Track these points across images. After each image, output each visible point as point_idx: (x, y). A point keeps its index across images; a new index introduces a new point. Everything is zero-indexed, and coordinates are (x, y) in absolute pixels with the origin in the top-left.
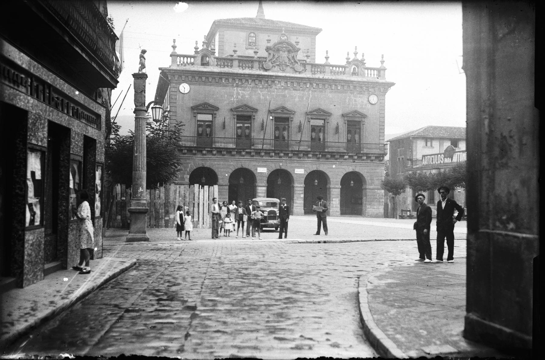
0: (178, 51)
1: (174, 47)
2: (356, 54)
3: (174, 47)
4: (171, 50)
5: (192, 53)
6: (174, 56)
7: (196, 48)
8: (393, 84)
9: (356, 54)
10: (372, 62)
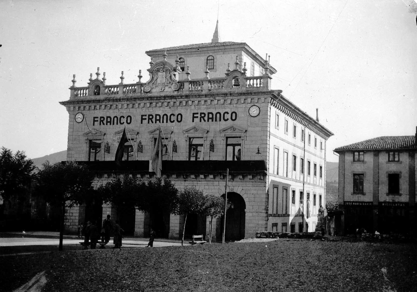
0: (77, 85)
1: (74, 82)
2: (98, 74)
3: (74, 82)
4: (71, 84)
5: (87, 85)
6: (73, 89)
8: (333, 135)
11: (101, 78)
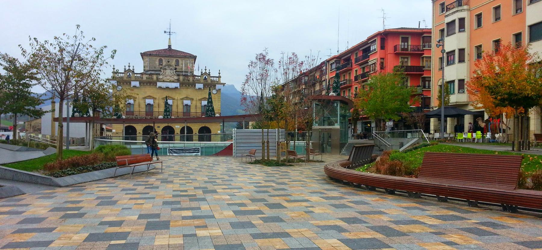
2: (206, 70)
7: (125, 69)
9: (206, 70)
10: (214, 73)
11: (131, 68)
